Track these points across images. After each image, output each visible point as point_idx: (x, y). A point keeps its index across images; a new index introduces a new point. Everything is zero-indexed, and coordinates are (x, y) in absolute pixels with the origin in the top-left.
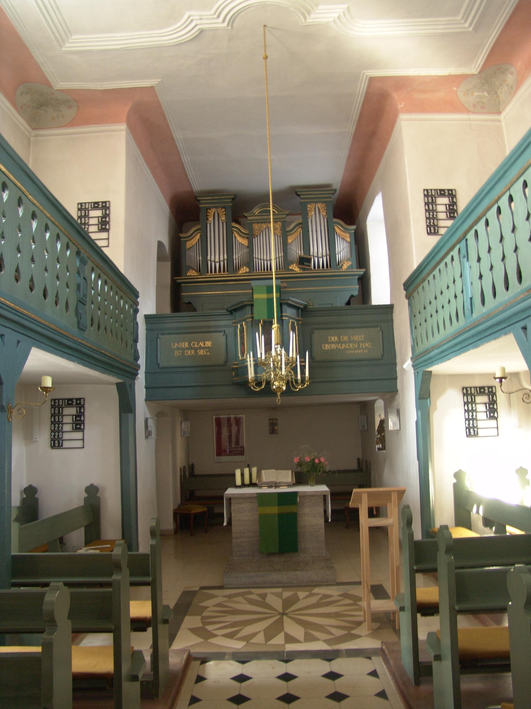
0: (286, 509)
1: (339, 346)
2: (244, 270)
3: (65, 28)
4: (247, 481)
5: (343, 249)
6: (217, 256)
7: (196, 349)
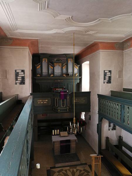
0: (68, 144)
1: (78, 101)
2: (52, 75)
3: (10, 22)
4: (56, 134)
5: (76, 70)
6: (45, 70)
7: (43, 102)
